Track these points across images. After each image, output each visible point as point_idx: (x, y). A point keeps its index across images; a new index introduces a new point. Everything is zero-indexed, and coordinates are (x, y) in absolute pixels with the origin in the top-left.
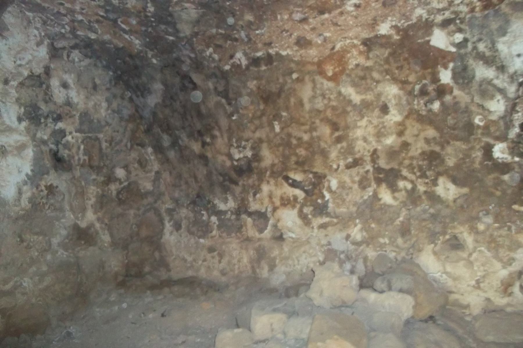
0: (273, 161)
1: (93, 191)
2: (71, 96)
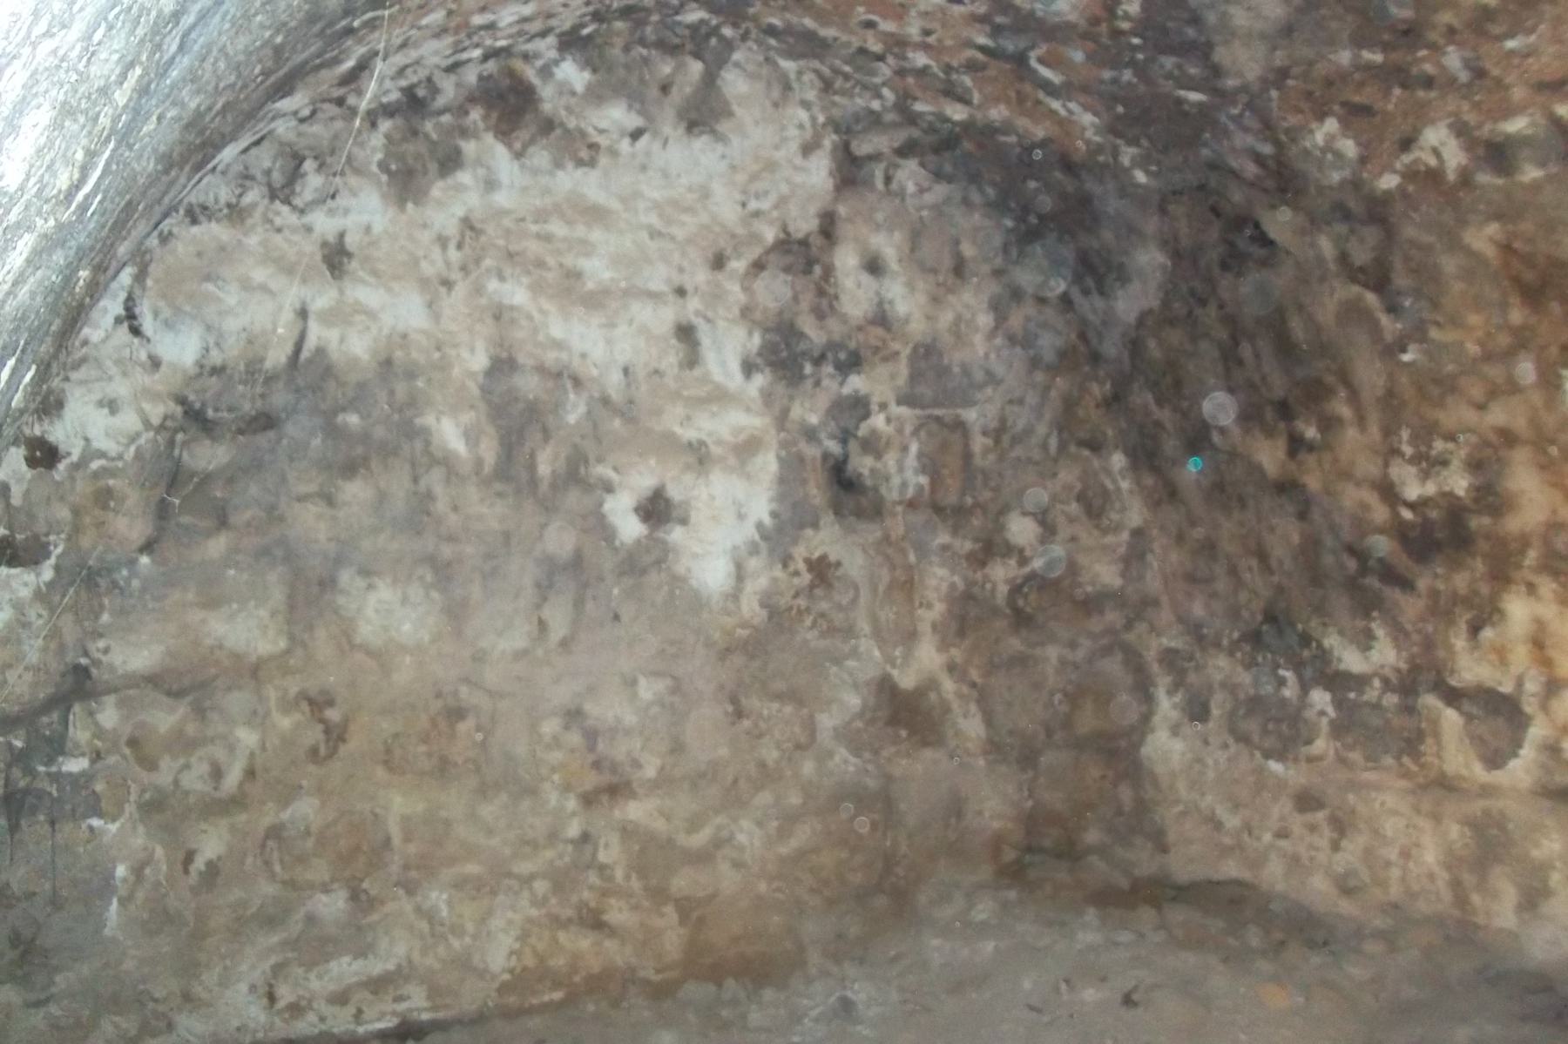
0: (1554, 512)
1: (939, 579)
2: (890, 296)
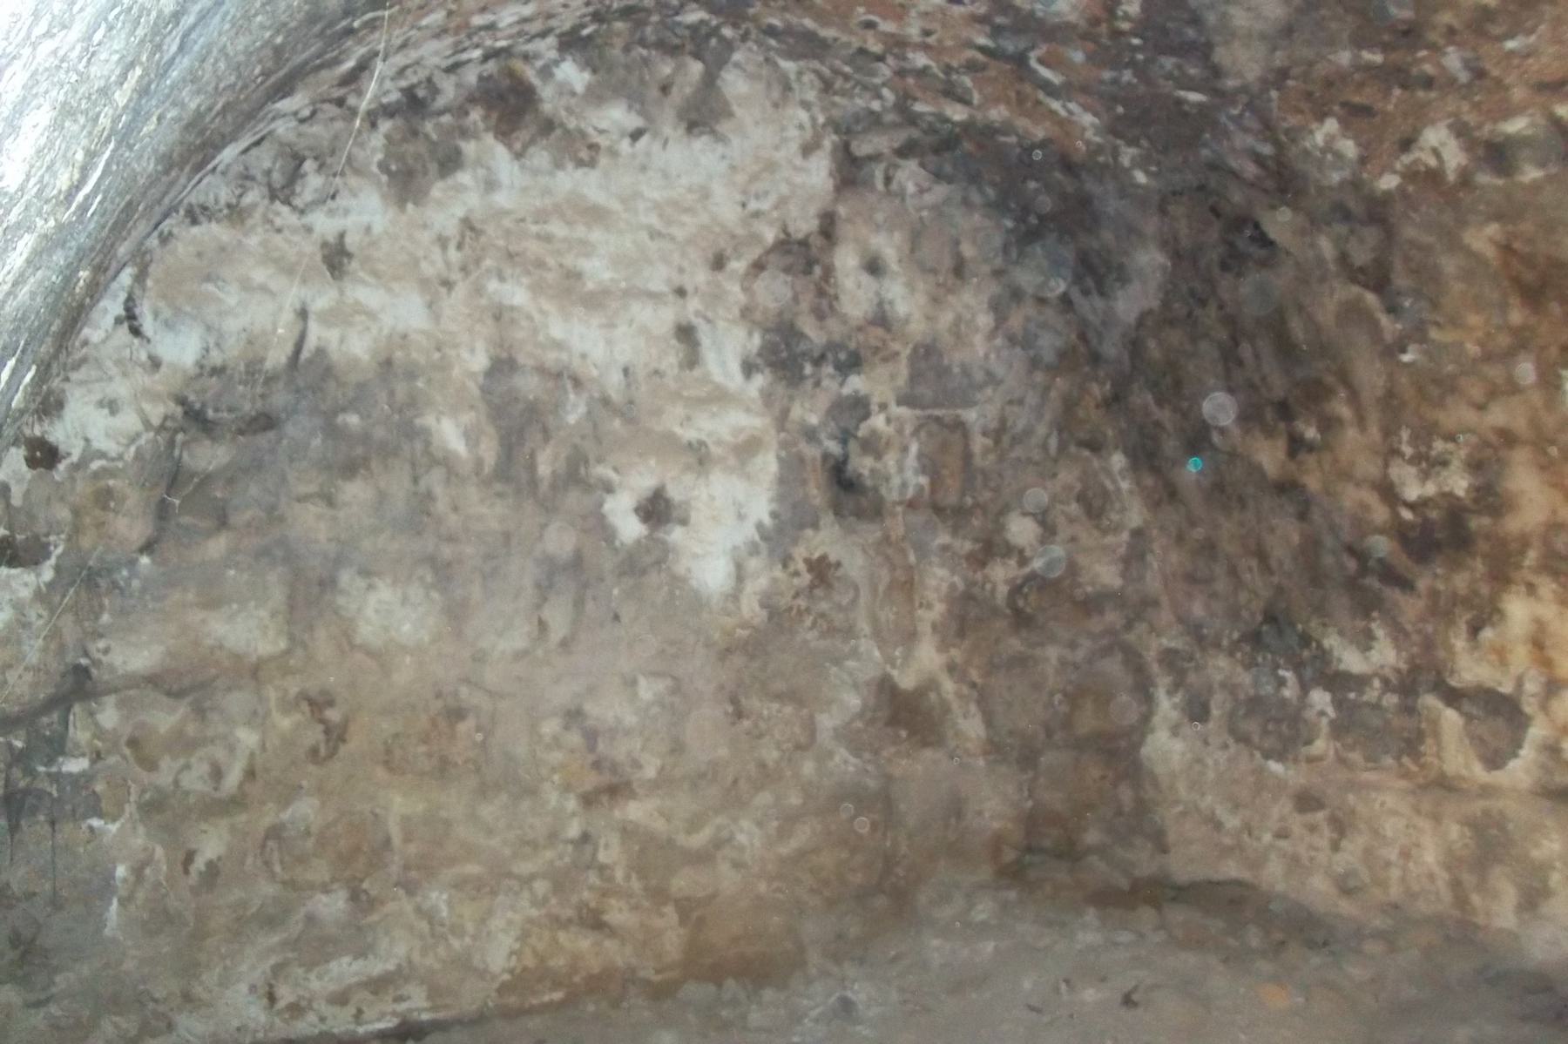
0: (1554, 512)
1: (939, 579)
2: (890, 296)
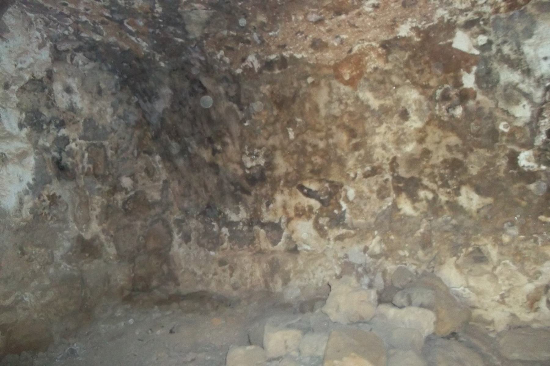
0: (287, 169)
1: (98, 201)
2: (75, 101)
